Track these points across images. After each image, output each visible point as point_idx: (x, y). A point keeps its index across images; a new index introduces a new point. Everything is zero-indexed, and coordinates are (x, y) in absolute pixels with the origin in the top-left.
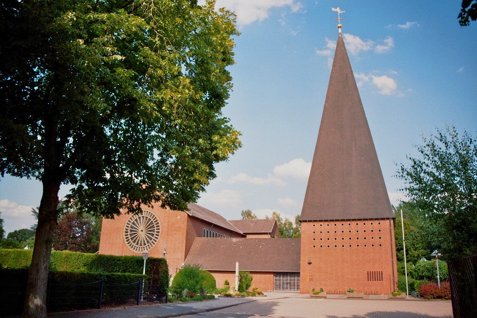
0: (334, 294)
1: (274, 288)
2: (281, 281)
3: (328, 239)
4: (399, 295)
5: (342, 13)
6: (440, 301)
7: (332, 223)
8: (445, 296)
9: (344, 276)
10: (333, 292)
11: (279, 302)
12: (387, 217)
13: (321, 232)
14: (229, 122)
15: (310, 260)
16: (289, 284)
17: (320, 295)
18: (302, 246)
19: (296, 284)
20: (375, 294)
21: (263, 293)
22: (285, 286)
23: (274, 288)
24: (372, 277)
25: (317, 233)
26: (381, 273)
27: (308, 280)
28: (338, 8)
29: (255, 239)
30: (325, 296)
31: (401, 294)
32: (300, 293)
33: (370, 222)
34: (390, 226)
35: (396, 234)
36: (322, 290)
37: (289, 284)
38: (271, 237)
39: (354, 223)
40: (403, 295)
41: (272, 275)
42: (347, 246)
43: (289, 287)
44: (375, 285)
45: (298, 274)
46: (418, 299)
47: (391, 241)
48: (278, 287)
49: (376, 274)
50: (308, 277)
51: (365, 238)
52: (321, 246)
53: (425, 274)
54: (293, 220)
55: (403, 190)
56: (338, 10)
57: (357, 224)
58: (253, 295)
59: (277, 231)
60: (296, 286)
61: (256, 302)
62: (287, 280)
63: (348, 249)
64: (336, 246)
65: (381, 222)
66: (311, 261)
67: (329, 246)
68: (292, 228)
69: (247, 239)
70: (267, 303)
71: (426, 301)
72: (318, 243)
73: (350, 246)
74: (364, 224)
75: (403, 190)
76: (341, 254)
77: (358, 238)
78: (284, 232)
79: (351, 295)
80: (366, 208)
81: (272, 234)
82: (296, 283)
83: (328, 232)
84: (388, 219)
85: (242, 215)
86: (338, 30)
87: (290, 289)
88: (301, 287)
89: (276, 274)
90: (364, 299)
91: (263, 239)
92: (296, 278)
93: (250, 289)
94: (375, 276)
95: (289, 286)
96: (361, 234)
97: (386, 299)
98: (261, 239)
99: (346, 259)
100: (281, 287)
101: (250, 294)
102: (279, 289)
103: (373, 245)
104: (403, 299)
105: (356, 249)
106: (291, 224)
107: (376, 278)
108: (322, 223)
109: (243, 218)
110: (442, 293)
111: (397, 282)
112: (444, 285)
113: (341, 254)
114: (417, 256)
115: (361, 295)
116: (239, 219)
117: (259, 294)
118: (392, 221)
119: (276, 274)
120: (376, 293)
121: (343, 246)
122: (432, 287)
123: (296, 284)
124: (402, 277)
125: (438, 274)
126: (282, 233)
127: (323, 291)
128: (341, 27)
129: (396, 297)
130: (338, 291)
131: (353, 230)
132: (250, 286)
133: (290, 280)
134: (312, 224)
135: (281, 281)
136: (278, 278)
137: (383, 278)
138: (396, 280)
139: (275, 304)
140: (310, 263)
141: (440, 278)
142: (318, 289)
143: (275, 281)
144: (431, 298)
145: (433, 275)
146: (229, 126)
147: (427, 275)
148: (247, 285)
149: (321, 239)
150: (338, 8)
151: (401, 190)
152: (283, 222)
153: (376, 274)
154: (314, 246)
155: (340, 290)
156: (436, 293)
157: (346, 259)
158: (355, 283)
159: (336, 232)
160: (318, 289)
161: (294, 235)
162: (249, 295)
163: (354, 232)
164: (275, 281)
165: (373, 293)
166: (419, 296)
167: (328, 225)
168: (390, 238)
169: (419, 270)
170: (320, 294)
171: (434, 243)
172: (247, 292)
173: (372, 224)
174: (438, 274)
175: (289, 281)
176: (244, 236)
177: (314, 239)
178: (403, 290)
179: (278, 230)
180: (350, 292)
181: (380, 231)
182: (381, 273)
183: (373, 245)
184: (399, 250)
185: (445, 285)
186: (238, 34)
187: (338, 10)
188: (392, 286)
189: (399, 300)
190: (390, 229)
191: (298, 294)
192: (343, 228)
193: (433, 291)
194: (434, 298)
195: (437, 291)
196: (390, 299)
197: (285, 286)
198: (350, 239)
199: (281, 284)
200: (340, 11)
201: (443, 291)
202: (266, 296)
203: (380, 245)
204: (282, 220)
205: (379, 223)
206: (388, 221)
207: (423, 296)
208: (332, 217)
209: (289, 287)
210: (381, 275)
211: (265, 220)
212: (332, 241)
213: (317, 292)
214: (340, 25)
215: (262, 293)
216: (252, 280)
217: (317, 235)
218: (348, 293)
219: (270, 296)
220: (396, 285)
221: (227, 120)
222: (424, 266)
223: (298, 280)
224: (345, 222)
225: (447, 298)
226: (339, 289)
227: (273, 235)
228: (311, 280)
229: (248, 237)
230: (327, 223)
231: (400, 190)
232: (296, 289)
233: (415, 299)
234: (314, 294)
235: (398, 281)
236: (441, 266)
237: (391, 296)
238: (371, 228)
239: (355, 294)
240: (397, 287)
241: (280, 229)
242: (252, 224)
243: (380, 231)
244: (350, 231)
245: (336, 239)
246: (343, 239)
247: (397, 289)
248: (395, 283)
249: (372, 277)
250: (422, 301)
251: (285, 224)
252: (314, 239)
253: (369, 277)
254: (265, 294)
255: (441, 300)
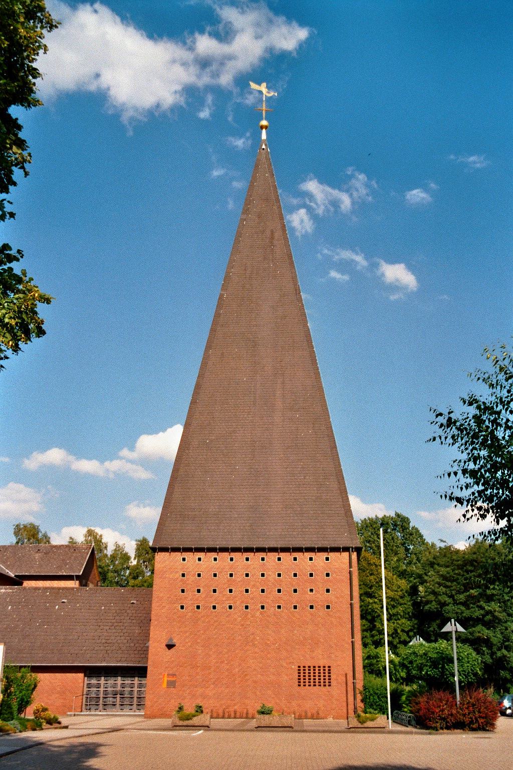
0: (223, 717)
1: (84, 706)
2: (102, 689)
3: (215, 591)
4: (373, 720)
5: (271, 97)
6: (461, 733)
7: (226, 554)
8: (471, 722)
9: (246, 675)
10: (221, 714)
11: (101, 745)
12: (344, 545)
13: (199, 575)
14: (18, 260)
15: (171, 639)
16: (118, 696)
17: (196, 721)
18: (155, 605)
19: (135, 695)
20: (312, 717)
21: (59, 720)
22: (110, 700)
23: (84, 706)
24: (307, 678)
25: (191, 578)
26: (327, 669)
27: (165, 685)
28: (264, 85)
29: (46, 589)
30: (207, 723)
31: (377, 718)
32: (146, 716)
33: (308, 555)
34: (350, 566)
35: (363, 584)
36: (200, 710)
37: (118, 696)
38: (81, 584)
39: (273, 556)
40: (382, 720)
41: (81, 675)
42: (255, 607)
43: (118, 703)
44: (315, 697)
45: (142, 672)
46: (410, 729)
47: (351, 599)
48: (92, 703)
49: (317, 671)
50: (166, 679)
51: (295, 591)
52: (198, 607)
53: (426, 673)
54: (131, 548)
55: (456, 474)
56: (263, 88)
57: (279, 559)
58: (37, 726)
59: (95, 572)
60: (135, 699)
61: (42, 746)
62: (115, 686)
63: (258, 613)
64: (230, 607)
65: (332, 555)
66: (175, 641)
67: (214, 607)
68: (128, 568)
69: (25, 588)
70: (71, 749)
71: (430, 734)
72: (190, 599)
73: (263, 607)
74: (295, 559)
75: (456, 474)
76: (242, 625)
77: (279, 591)
78: (110, 575)
79: (266, 720)
80: (300, 524)
81: (83, 580)
82: (136, 692)
83: (215, 575)
84: (346, 549)
85: (16, 533)
86: (261, 134)
87: (122, 707)
88: (148, 703)
89: (91, 672)
90: (296, 731)
91: (63, 589)
92: (136, 681)
93: (29, 714)
94: (313, 676)
95: (118, 699)
96: (287, 582)
97: (343, 728)
98: (59, 589)
99: (252, 637)
100: (101, 702)
101: (29, 725)
102: (97, 707)
103: (312, 607)
104: (381, 730)
105: (274, 615)
106: (126, 558)
107: (317, 681)
108: (201, 555)
109: (17, 543)
110: (464, 715)
111: (361, 689)
112: (469, 698)
113: (242, 625)
114: (393, 634)
115: (289, 720)
116: (7, 543)
117: (51, 724)
118: (355, 553)
119: (91, 672)
120: (316, 716)
121: (247, 607)
122: (444, 702)
123: (135, 695)
124: (375, 681)
125: (457, 673)
126: (104, 577)
127: (202, 712)
128: (266, 127)
129: (366, 725)
130: (232, 709)
131: (270, 573)
132: (28, 703)
133: (123, 686)
134: (178, 556)
135: (102, 689)
136: (94, 681)
137: (332, 681)
138: (360, 686)
139: (91, 751)
140: (170, 647)
141: (460, 682)
142: (189, 709)
143: (86, 689)
144: (442, 728)
145: (443, 673)
146: (17, 271)
147: (430, 675)
148: (22, 700)
149: (199, 591)
150: (264, 85)
151: (452, 474)
152: (109, 551)
153: (317, 671)
154: (182, 607)
155: (236, 707)
156: (452, 715)
157: (252, 637)
158: (269, 692)
159: (231, 575)
160: (189, 709)
161: (132, 582)
162: (25, 729)
163: (272, 576)
164: (86, 689)
165: (309, 714)
166: (413, 722)
167: (215, 559)
168: (349, 593)
169: (411, 662)
170: (195, 719)
171: (429, 606)
172: (21, 719)
173: (311, 559)
174: (457, 673)
175: (119, 688)
176: (17, 581)
177: (183, 591)
178: (375, 707)
179: (94, 567)
180: (263, 713)
181: (328, 575)
182: (327, 669)
183: (312, 607)
184: (370, 617)
185: (471, 698)
186: (36, 103)
187: (263, 88)
188: (351, 698)
189: (370, 732)
190: (350, 572)
191: (139, 719)
192: (248, 567)
193: (446, 712)
194: (448, 728)
195: (454, 712)
196: (350, 730)
197: (110, 700)
198: (263, 591)
199: (101, 695)
200: (268, 93)
201: (467, 711)
202: (66, 727)
203: (328, 607)
204: (106, 548)
205: (327, 559)
206: (346, 555)
207: (423, 722)
208: (224, 543)
209: (118, 703)
210: (327, 674)
211: (67, 546)
212: (224, 595)
213: (188, 715)
214: (264, 123)
215: (57, 719)
216: (35, 686)
217: (190, 582)
218: (257, 716)
219: (79, 727)
220: (359, 697)
221: (13, 252)
222: (425, 654)
223: (140, 686)
224: (301, 554)
225: (474, 726)
226: (235, 705)
227: (84, 581)
228: (171, 684)
229: (27, 584)
230: (214, 555)
231: (449, 475)
232: (135, 706)
233: (403, 728)
234: (181, 719)
235: (364, 687)
236: (462, 654)
237: (354, 722)
238: (309, 569)
239: (273, 719)
240: (362, 701)
241: (100, 567)
242: (37, 556)
243: (328, 575)
244: (263, 575)
245: (231, 591)
246: (247, 591)
247: (362, 705)
248: (357, 692)
249: (307, 678)
250: (422, 734)
251: (113, 557)
252: (183, 591)
253: (302, 677)
254: (64, 721)
255: (462, 731)
